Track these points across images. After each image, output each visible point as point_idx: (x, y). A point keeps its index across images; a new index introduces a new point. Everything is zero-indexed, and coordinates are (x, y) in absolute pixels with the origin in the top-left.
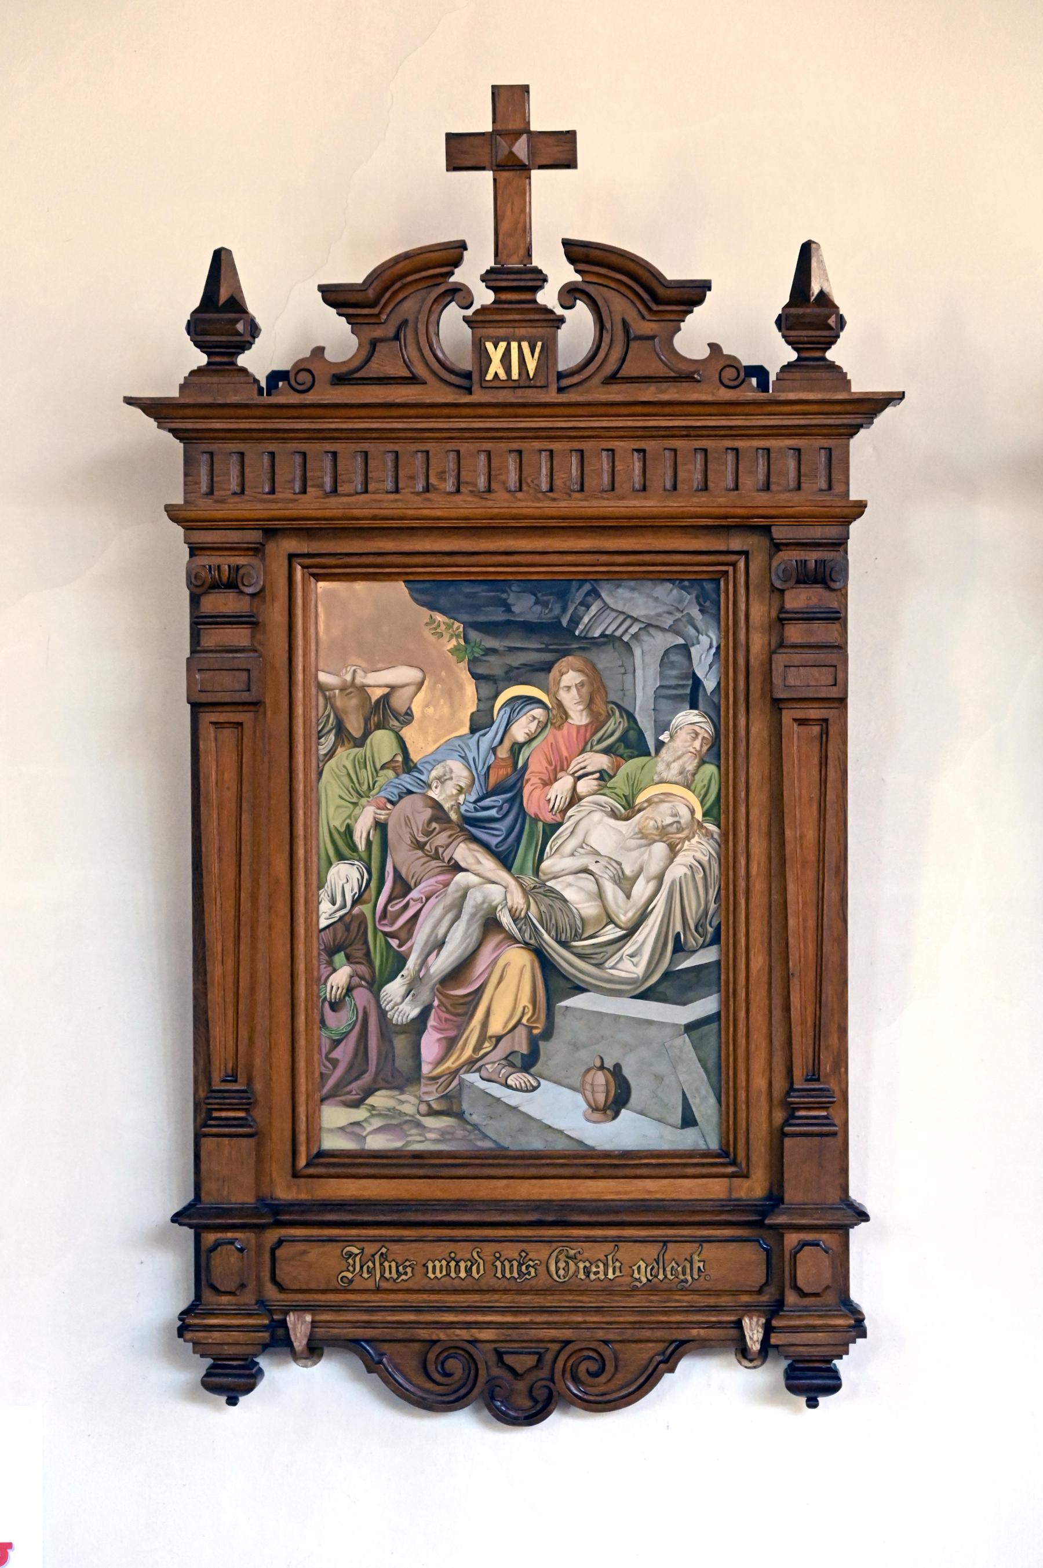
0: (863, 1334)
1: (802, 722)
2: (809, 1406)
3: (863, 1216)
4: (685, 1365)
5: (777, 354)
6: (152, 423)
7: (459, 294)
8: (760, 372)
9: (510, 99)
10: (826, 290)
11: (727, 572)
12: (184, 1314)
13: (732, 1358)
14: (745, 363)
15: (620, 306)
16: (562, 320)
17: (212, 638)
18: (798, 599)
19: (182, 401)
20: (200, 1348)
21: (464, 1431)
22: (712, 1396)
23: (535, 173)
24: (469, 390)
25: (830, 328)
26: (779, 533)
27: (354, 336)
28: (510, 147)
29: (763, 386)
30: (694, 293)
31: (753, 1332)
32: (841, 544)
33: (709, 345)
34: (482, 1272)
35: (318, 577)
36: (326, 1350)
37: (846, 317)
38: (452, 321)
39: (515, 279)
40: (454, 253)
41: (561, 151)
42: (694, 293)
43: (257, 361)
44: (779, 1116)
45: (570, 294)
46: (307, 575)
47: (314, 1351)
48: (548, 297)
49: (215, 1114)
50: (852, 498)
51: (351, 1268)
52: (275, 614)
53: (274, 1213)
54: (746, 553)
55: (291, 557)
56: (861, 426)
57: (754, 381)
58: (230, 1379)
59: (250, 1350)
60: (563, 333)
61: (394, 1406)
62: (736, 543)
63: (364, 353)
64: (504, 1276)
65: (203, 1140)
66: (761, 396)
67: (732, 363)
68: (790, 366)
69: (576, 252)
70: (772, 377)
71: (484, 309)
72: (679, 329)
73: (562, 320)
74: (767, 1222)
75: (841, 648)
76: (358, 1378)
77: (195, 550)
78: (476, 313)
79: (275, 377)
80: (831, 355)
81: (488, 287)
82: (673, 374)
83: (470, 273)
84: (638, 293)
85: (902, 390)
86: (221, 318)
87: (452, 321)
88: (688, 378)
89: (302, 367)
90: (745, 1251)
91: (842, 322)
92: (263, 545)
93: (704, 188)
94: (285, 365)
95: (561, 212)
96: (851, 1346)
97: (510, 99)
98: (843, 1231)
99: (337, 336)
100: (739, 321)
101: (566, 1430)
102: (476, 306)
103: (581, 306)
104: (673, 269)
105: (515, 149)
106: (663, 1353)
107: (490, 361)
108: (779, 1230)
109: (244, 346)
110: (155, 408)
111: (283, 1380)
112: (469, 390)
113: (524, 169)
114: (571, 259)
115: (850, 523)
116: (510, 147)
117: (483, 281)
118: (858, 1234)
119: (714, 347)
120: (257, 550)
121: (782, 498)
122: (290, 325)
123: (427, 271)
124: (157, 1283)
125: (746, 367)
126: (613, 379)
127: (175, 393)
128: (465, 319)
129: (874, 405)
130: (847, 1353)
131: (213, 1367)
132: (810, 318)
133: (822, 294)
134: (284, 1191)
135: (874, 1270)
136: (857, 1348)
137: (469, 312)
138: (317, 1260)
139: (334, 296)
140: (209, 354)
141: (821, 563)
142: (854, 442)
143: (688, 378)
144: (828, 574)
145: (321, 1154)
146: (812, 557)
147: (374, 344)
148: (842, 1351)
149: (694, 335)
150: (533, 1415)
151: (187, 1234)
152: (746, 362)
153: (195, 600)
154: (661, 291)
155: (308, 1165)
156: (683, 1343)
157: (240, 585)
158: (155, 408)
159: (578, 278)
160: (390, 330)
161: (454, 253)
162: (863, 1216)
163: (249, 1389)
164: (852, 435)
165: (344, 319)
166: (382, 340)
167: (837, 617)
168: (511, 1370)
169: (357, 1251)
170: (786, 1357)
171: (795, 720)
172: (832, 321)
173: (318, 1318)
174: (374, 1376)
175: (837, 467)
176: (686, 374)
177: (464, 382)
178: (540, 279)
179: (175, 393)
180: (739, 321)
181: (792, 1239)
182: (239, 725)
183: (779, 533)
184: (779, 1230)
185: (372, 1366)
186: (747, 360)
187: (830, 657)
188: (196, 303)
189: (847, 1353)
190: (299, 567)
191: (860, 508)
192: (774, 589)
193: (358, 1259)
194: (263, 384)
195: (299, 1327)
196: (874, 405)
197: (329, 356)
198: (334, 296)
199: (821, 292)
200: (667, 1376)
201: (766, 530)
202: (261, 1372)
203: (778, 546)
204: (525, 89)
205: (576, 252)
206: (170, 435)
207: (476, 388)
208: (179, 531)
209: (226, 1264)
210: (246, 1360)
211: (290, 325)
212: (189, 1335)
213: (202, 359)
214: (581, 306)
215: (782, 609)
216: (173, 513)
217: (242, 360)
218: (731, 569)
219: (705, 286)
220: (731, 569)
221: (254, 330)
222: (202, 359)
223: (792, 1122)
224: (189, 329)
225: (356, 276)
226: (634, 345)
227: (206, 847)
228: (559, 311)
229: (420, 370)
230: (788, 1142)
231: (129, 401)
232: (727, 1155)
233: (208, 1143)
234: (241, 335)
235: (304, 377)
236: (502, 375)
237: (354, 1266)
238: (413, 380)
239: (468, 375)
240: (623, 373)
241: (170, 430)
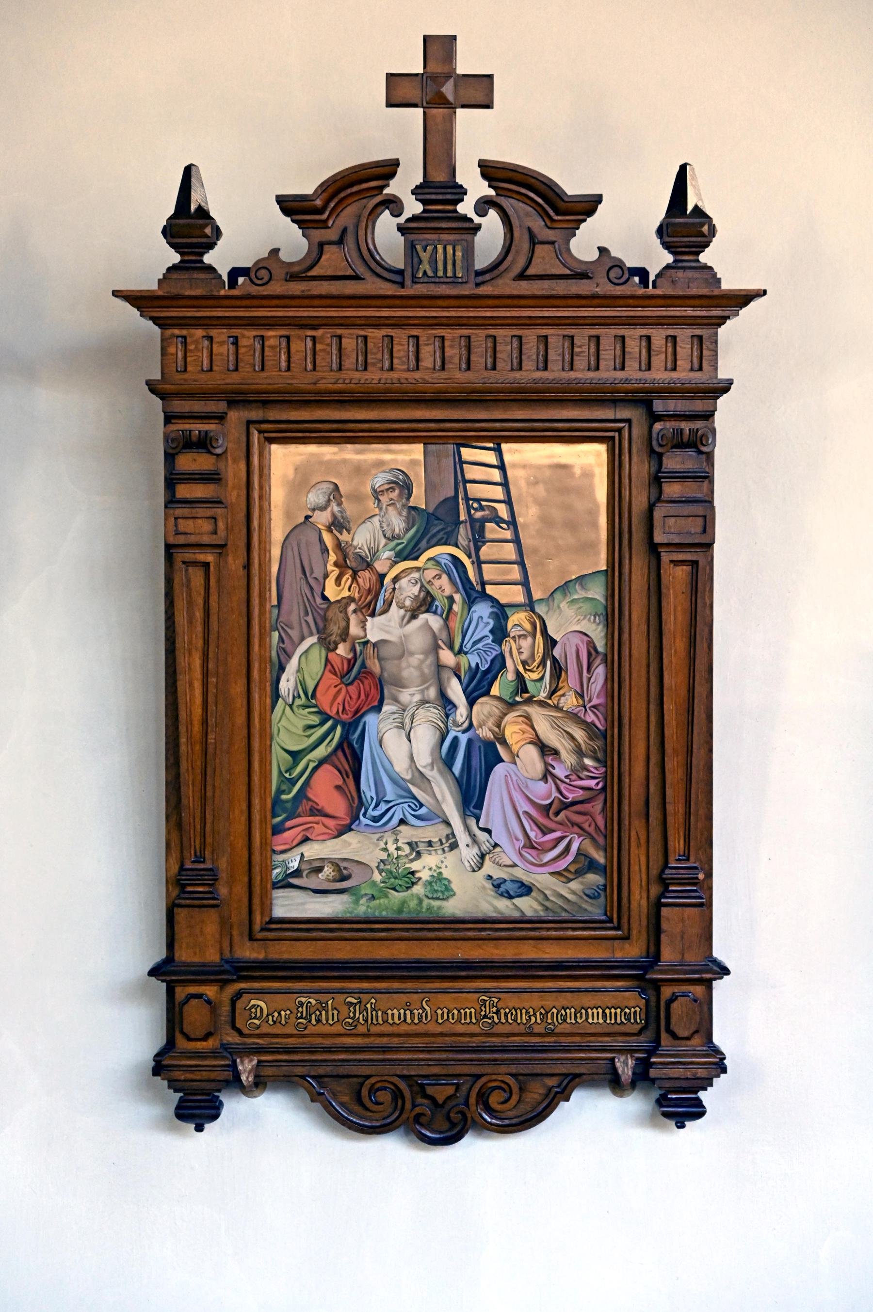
0: (724, 1070)
1: (677, 563)
2: (679, 1127)
3: (725, 971)
4: (577, 1096)
5: (658, 259)
6: (136, 312)
7: (394, 205)
8: (642, 273)
9: (440, 48)
10: (700, 204)
11: (613, 438)
12: (159, 1057)
13: (608, 1092)
14: (629, 265)
15: (528, 217)
16: (478, 227)
17: (183, 491)
18: (673, 462)
19: (161, 293)
20: (174, 1085)
21: (392, 1156)
22: (596, 1126)
23: (459, 111)
24: (402, 285)
25: (704, 235)
26: (658, 406)
27: (304, 239)
28: (438, 86)
29: (644, 281)
30: (589, 205)
31: (625, 1067)
32: (708, 416)
33: (599, 248)
34: (429, 1018)
35: (272, 441)
36: (268, 1084)
37: (718, 227)
38: (386, 231)
39: (441, 191)
40: (388, 170)
41: (480, 92)
42: (589, 205)
43: (220, 259)
44: (655, 890)
45: (483, 205)
46: (262, 439)
47: (260, 1084)
48: (466, 208)
49: (189, 889)
50: (719, 377)
51: (352, 1015)
52: (234, 472)
53: (241, 970)
54: (629, 421)
55: (249, 423)
56: (728, 317)
57: (637, 279)
58: (197, 1108)
59: (212, 1085)
60: (479, 237)
61: (334, 1130)
62: (624, 413)
63: (314, 255)
64: (586, 1011)
65: (176, 910)
66: (641, 291)
67: (619, 264)
68: (668, 267)
69: (490, 171)
70: (652, 278)
71: (414, 218)
72: (575, 235)
73: (478, 227)
74: (647, 977)
75: (708, 502)
76: (307, 1109)
77: (169, 418)
78: (408, 220)
79: (235, 273)
80: (704, 258)
81: (417, 199)
82: (568, 272)
83: (403, 186)
84: (541, 203)
85: (763, 288)
86: (190, 227)
87: (386, 231)
88: (583, 276)
89: (260, 265)
90: (589, 994)
91: (713, 231)
92: (226, 413)
93: (598, 119)
94: (247, 262)
95: (477, 137)
96: (715, 1080)
97: (440, 48)
98: (708, 985)
99: (291, 240)
100: (625, 229)
101: (474, 1149)
102: (407, 214)
103: (492, 213)
104: (572, 186)
105: (444, 90)
106: (559, 1086)
107: (420, 262)
108: (657, 985)
109: (211, 246)
110: (137, 300)
111: (234, 1106)
112: (402, 285)
113: (452, 107)
114: (484, 176)
115: (718, 397)
116: (438, 86)
117: (413, 194)
118: (719, 987)
119: (603, 250)
120: (221, 418)
121: (659, 375)
122: (249, 230)
123: (363, 184)
124: (133, 1032)
125: (629, 269)
126: (522, 276)
127: (154, 286)
128: (400, 228)
129: (744, 298)
130: (711, 1085)
131: (181, 1100)
132: (685, 227)
133: (696, 208)
134: (249, 952)
135: (735, 1018)
136: (720, 1082)
137: (402, 220)
138: (265, 1009)
139: (289, 206)
140: (181, 254)
141: (693, 432)
142: (722, 331)
143: (583, 276)
144: (699, 444)
145: (272, 921)
146: (686, 426)
147: (321, 245)
148: (707, 1083)
149: (584, 244)
150: (450, 1137)
151: (161, 987)
152: (629, 264)
153: (170, 457)
154: (561, 205)
155: (262, 930)
156: (579, 1075)
157: (209, 446)
158: (137, 300)
159: (492, 192)
160: (332, 234)
161: (388, 170)
162: (725, 971)
163: (215, 1117)
164: (720, 325)
165: (295, 226)
166: (330, 243)
167: (706, 477)
168: (432, 1099)
169: (356, 1001)
170: (660, 1088)
171: (671, 561)
172: (705, 229)
173: (263, 1058)
174: (318, 1105)
175: (705, 350)
176: (582, 274)
177: (397, 278)
178: (460, 192)
179: (154, 286)
180: (625, 229)
181: (667, 992)
182: (206, 565)
183: (658, 406)
184: (657, 985)
185: (315, 1097)
186: (631, 262)
187: (699, 509)
188: (172, 211)
189: (711, 1085)
190: (256, 432)
191: (725, 387)
192: (652, 451)
193: (357, 1007)
194: (225, 278)
195: (246, 1067)
196: (744, 298)
197: (284, 256)
198: (289, 206)
199: (696, 207)
200: (563, 1105)
201: (648, 404)
202: (221, 1103)
203: (654, 417)
204: (454, 38)
205: (490, 171)
206: (151, 322)
207: (408, 282)
208: (158, 402)
209: (195, 1016)
210: (208, 1094)
211: (249, 230)
212: (164, 1073)
213: (176, 258)
214: (492, 213)
215: (659, 470)
216: (152, 387)
217: (208, 259)
218: (617, 434)
219: (597, 200)
220: (617, 434)
221: (218, 233)
222: (176, 258)
223: (668, 895)
224: (164, 232)
225: (308, 188)
226: (539, 249)
227: (492, 784)
228: (477, 219)
229: (361, 270)
230: (665, 911)
231: (116, 294)
232: (611, 921)
233: (181, 915)
234: (209, 237)
235: (263, 273)
236: (430, 273)
237: (354, 1013)
238: (356, 277)
239: (401, 272)
240: (531, 271)
241: (152, 318)
